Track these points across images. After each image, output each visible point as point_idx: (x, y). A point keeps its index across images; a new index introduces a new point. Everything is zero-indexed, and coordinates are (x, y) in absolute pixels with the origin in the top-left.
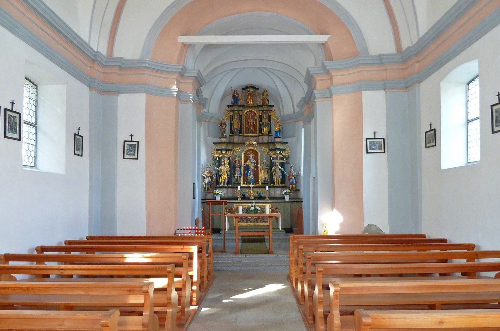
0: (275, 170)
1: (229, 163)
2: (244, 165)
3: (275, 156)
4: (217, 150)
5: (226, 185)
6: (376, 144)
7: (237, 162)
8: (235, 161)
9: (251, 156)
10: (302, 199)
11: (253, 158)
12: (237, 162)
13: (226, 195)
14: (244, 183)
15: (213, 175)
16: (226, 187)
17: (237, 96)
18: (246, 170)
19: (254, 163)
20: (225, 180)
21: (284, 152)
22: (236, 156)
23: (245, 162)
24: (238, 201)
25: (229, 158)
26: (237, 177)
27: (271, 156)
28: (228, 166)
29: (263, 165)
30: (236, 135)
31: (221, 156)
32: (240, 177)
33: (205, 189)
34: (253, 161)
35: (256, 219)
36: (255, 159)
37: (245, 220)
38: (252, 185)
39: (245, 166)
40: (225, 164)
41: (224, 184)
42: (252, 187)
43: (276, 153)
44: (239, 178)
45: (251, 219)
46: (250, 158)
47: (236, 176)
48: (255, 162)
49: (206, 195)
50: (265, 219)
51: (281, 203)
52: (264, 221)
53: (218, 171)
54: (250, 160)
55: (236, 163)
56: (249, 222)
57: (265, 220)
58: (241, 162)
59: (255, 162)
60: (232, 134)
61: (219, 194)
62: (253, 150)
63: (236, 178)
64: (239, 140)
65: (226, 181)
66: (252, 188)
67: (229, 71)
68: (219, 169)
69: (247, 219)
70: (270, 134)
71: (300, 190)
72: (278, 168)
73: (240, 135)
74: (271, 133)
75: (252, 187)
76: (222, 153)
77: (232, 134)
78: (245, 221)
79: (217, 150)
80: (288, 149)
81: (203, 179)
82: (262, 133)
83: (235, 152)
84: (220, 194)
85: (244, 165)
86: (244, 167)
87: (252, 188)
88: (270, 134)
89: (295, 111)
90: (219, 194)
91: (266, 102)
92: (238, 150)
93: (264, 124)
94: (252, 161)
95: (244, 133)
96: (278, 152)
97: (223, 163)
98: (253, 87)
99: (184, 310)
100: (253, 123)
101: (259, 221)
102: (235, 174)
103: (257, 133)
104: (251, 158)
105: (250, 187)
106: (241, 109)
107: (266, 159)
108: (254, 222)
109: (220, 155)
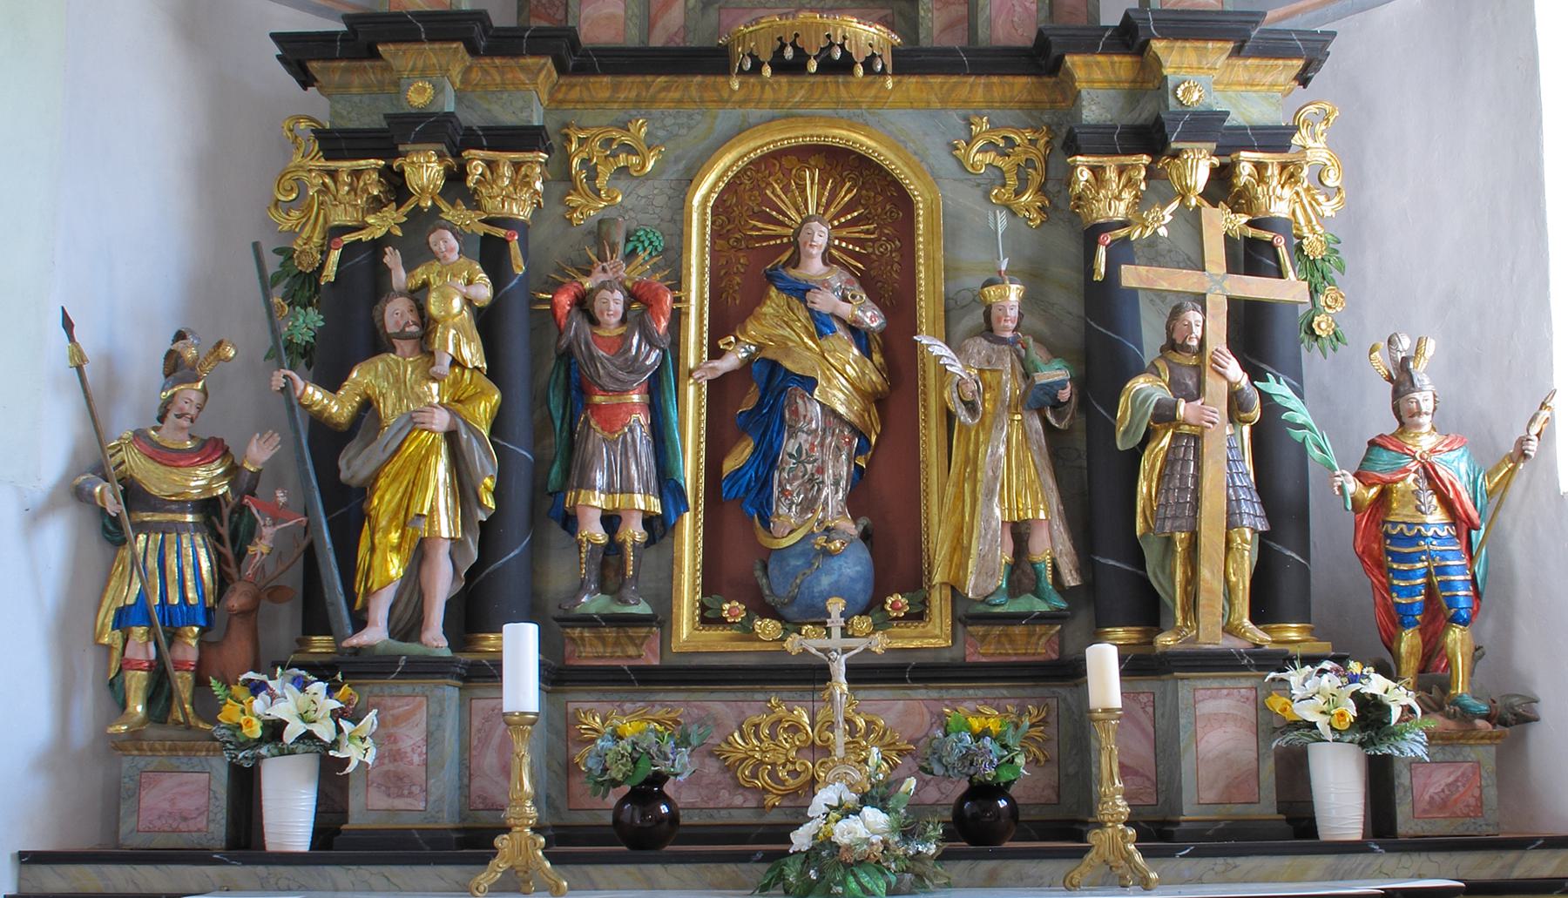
0: (1165, 416)
1: (487, 322)
2: (716, 353)
3: (1163, 219)
4: (335, 143)
5: (435, 638)
7: (613, 304)
8: (584, 303)
9: (819, 235)
12: (613, 304)
13: (446, 782)
14: (708, 618)
16: (426, 668)
18: (739, 438)
19: (858, 333)
20: (419, 555)
22: (599, 235)
23: (722, 324)
25: (491, 255)
26: (611, 521)
28: (472, 353)
31: (382, 223)
32: (659, 528)
38: (836, 639)
40: (427, 324)
41: (407, 624)
42: (839, 669)
43: (1160, 186)
44: (634, 532)
46: (795, 261)
47: (598, 500)
48: (872, 318)
49: (116, 799)
55: (594, 321)
58: (677, 318)
59: (872, 318)
61: (290, 735)
63: (601, 536)
64: (649, 24)
66: (840, 685)
67: (554, 376)
68: (338, 407)
75: (839, 669)
76: (396, 187)
79: (335, 143)
80: (1314, 146)
81: (95, 546)
83: (593, 175)
84: (309, 736)
85: (716, 353)
86: (718, 389)
87: (840, 685)
89: (1155, 41)
90: (294, 729)
92: (631, 150)
94: (825, 301)
96: (1199, 168)
97: (396, 314)
99: (859, 348)
104: (815, 266)
105: (813, 675)
107: (1034, 278)
109: (376, 205)
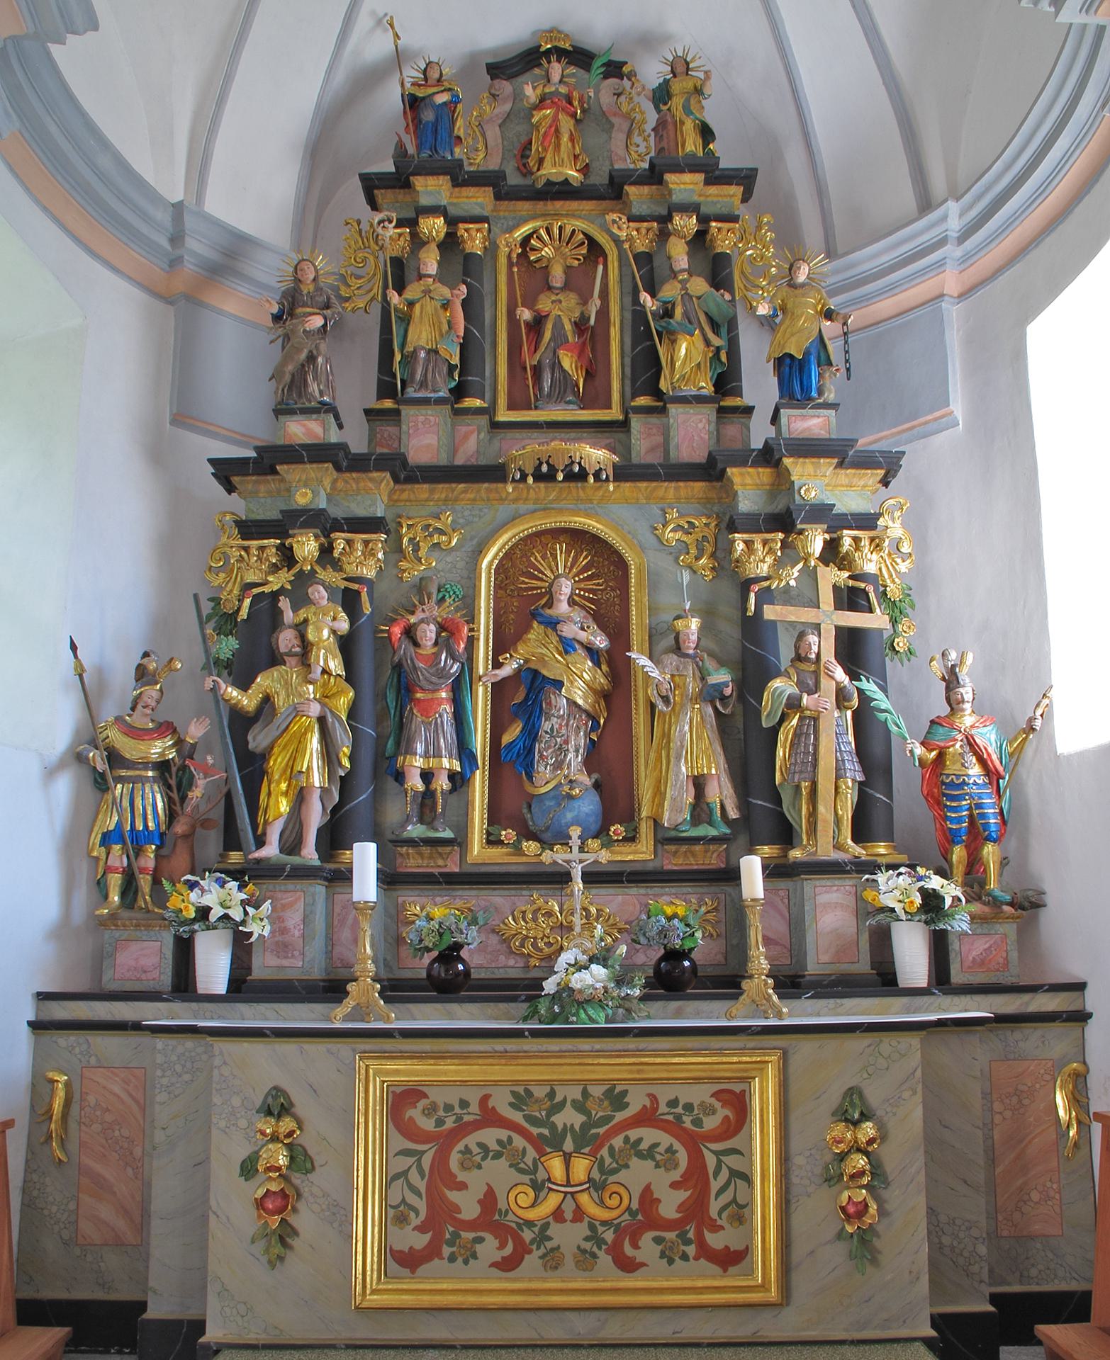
0: (793, 704)
1: (346, 645)
2: (497, 665)
4: (248, 529)
5: (310, 854)
6: (605, 988)
7: (429, 633)
8: (409, 632)
9: (566, 587)
10: (1080, 987)
11: (583, 607)
12: (429, 633)
15: (186, 751)
17: (442, 98)
21: (865, 543)
22: (420, 587)
23: (502, 646)
24: (338, 1016)
25: (349, 601)
26: (427, 776)
27: (746, 585)
28: (336, 665)
29: (672, 660)
30: (425, 402)
32: (459, 781)
33: (101, 887)
34: (578, 626)
35: (609, 1236)
36: (600, 618)
37: (491, 1242)
39: (506, 671)
40: (306, 647)
41: (292, 844)
43: (790, 553)
44: (442, 783)
45: (555, 1230)
46: (550, 604)
47: (419, 762)
48: (601, 642)
49: (100, 959)
50: (716, 1228)
51: (888, 1042)
52: (705, 1252)
53: (241, 722)
54: (553, 624)
55: (416, 644)
56: (532, 1261)
57: (715, 1241)
58: (472, 642)
59: (601, 642)
60: (388, 404)
62: (579, 538)
63: (420, 786)
65: (315, 817)
66: (578, 884)
69: (502, 1231)
70: (729, 402)
71: (1050, 899)
72: (824, 681)
73: (467, 411)
74: (738, 392)
76: (288, 556)
77: (388, 404)
78: (490, 1248)
79: (248, 529)
80: (893, 527)
81: (90, 793)
82: (658, 394)
83: (416, 549)
85: (497, 665)
86: (499, 689)
87: (578, 884)
88: (729, 402)
91: (692, 144)
92: (442, 532)
93: (679, 311)
94: (569, 630)
95: (502, 401)
96: (816, 541)
97: (286, 640)
98: (579, 57)
100: (580, 325)
101: (647, 1248)
102: (403, 743)
103: (616, 396)
104: (563, 607)
105: (560, 878)
106: (479, 200)
107: (708, 615)
108: (586, 1259)
109: (275, 569)
